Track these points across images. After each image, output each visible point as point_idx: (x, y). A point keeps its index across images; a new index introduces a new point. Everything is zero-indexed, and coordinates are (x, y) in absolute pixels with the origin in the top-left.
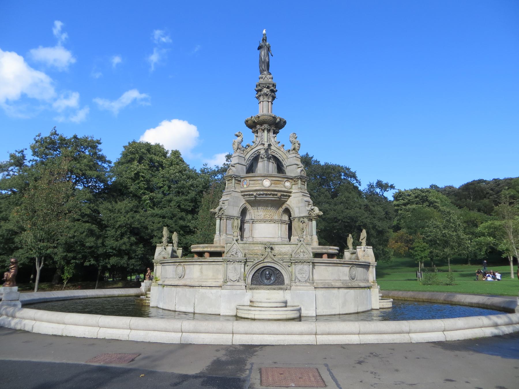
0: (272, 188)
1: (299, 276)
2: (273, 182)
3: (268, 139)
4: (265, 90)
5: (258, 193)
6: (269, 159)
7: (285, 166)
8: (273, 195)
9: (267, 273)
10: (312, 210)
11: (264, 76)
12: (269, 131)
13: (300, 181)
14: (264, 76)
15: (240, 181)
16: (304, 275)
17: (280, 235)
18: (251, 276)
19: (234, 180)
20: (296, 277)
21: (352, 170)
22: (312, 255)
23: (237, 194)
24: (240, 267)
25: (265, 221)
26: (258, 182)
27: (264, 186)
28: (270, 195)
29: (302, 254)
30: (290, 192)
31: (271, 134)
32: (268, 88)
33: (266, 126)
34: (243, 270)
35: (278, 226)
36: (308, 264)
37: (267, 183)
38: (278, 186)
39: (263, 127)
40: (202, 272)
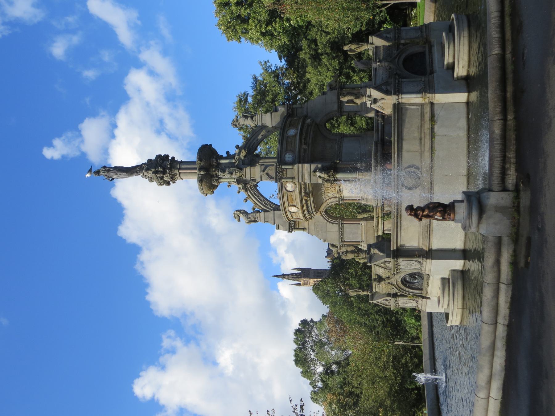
38: (294, 198)
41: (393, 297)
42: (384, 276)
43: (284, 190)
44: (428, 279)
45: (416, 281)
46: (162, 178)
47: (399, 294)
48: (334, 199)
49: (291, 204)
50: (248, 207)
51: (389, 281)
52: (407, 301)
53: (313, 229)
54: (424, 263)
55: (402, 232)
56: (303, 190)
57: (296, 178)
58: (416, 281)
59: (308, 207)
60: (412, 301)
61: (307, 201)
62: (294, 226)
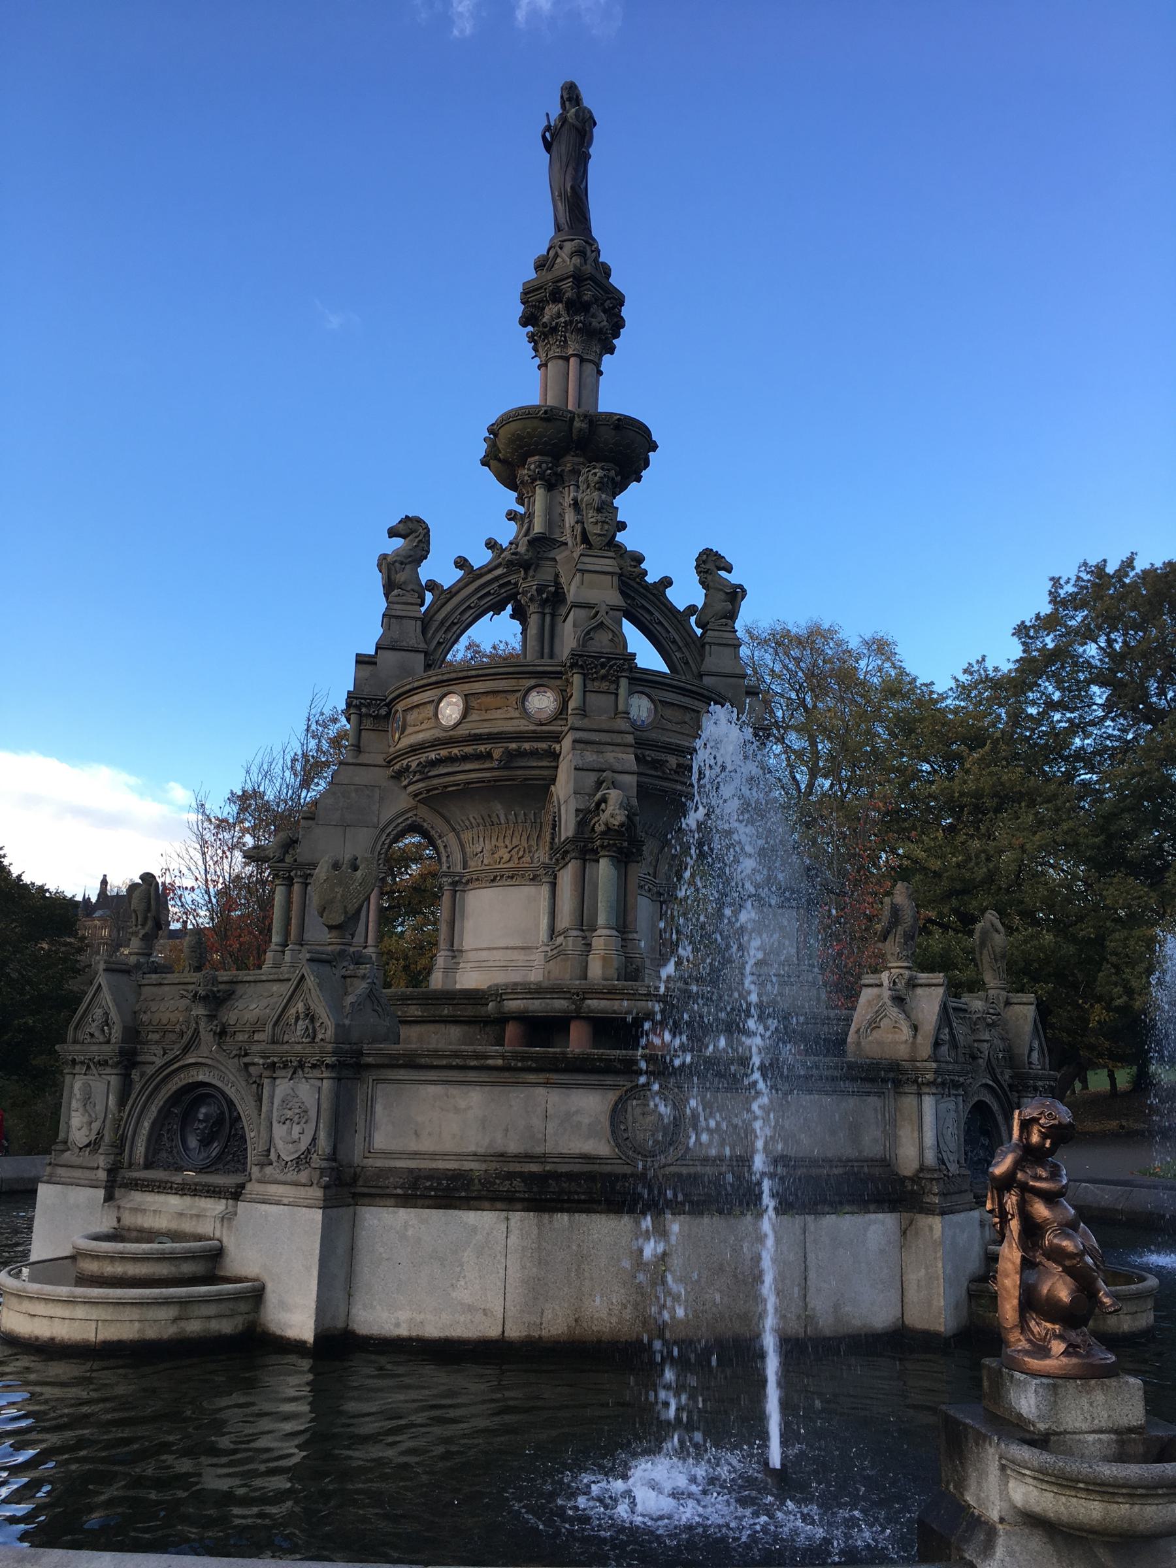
8: (479, 757)
38: (498, 714)
41: (122, 1052)
42: (231, 1016)
43: (532, 682)
44: (213, 1192)
45: (193, 1142)
46: (556, 296)
47: (135, 1075)
48: (457, 856)
49: (474, 703)
50: (438, 569)
51: (206, 1037)
52: (100, 1108)
53: (357, 780)
54: (303, 1176)
55: (439, 1089)
56: (527, 746)
57: (586, 723)
58: (193, 1142)
59: (465, 758)
60: (96, 1126)
61: (479, 757)
62: (368, 715)
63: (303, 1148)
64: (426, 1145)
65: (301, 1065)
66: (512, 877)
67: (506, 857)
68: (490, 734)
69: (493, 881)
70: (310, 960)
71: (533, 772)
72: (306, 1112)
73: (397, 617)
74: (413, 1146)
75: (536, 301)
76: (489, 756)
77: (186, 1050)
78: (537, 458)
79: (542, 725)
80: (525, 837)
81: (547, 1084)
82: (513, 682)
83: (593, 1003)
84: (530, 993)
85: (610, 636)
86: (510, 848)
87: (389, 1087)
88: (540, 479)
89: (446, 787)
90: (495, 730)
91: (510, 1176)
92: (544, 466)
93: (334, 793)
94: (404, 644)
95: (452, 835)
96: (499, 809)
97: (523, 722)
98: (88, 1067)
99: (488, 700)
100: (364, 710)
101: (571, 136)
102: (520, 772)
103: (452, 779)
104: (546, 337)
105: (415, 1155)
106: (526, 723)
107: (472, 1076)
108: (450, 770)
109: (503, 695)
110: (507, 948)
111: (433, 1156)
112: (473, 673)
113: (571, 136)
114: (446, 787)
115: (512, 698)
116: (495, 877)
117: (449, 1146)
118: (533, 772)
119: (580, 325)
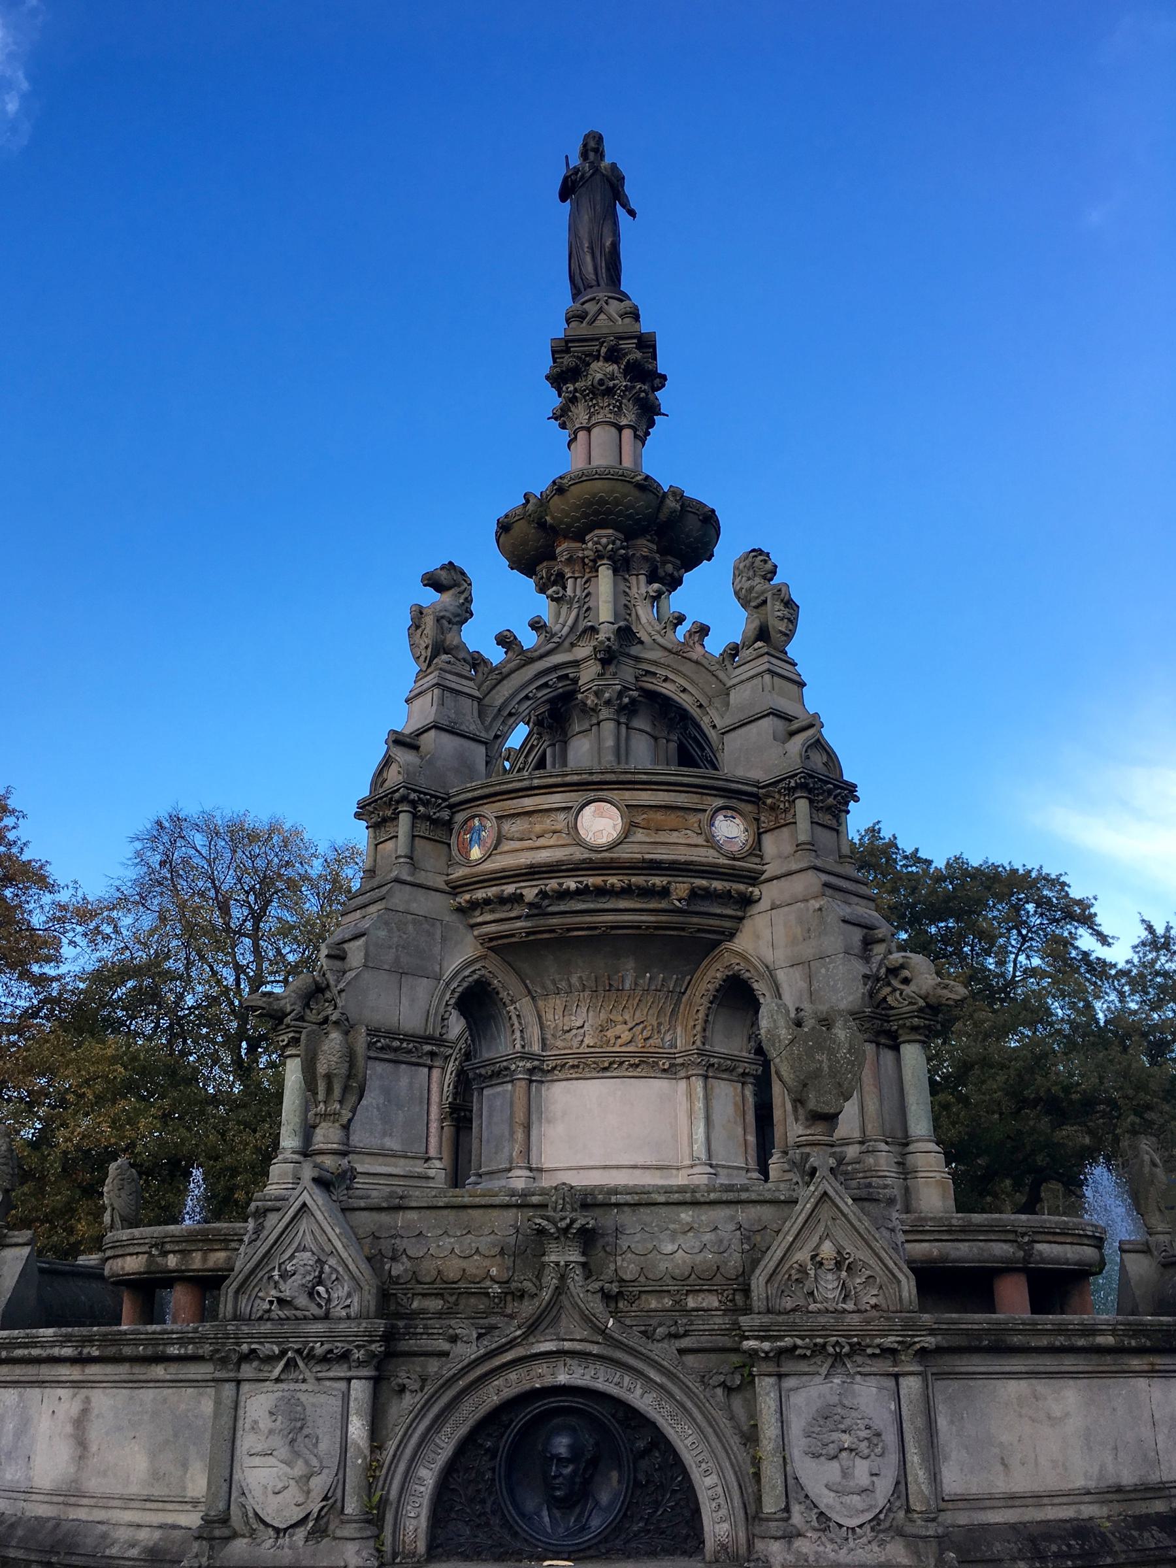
0: (626, 853)
1: (818, 1477)
2: (633, 818)
3: (624, 609)
4: (599, 370)
5: (553, 884)
6: (627, 710)
7: (712, 735)
8: (647, 893)
9: (561, 1445)
10: (893, 971)
11: (591, 308)
12: (622, 567)
13: (802, 806)
14: (591, 308)
15: (448, 825)
16: (861, 1470)
17: (700, 1149)
18: (428, 1476)
19: (404, 820)
20: (792, 1487)
21: (1076, 892)
22: (908, 1287)
23: (425, 904)
24: (340, 1411)
25: (605, 1065)
26: (547, 823)
27: (580, 843)
28: (626, 892)
29: (828, 1286)
30: (754, 878)
31: (640, 587)
32: (613, 356)
33: (603, 537)
34: (357, 1429)
35: (690, 1095)
36: (886, 1366)
37: (600, 824)
38: (674, 837)
39: (589, 548)
40: (81, 1443)
43: (720, 802)
48: (534, 1032)
52: (328, 1445)
53: (414, 907)
56: (717, 885)
59: (626, 892)
60: (319, 1484)
63: (881, 1502)
64: (1020, 1483)
65: (857, 1349)
66: (637, 1066)
67: (626, 1036)
68: (674, 862)
69: (605, 1069)
70: (314, 1180)
71: (711, 922)
72: (878, 1435)
73: (452, 690)
74: (1001, 1485)
75: (583, 352)
76: (665, 892)
77: (533, 1328)
78: (611, 531)
79: (734, 859)
80: (654, 1011)
81: (1152, 1373)
82: (695, 798)
83: (1044, 1249)
84: (948, 1232)
85: (825, 760)
86: (630, 1025)
87: (954, 1385)
88: (609, 558)
89: (569, 930)
90: (682, 858)
91: (1142, 1522)
92: (618, 542)
93: (387, 923)
94: (463, 727)
95: (527, 1000)
96: (628, 971)
97: (711, 852)
98: (291, 1365)
99: (659, 816)
100: (421, 809)
101: (594, 187)
102: (695, 920)
103: (588, 919)
104: (595, 397)
105: (1012, 1500)
106: (716, 854)
107: (1069, 1363)
108: (591, 906)
109: (681, 814)
110: (635, 1167)
111: (1038, 1499)
112: (644, 778)
113: (594, 187)
114: (569, 930)
115: (693, 819)
116: (611, 1063)
117: (1051, 1481)
118: (711, 922)
119: (643, 395)
